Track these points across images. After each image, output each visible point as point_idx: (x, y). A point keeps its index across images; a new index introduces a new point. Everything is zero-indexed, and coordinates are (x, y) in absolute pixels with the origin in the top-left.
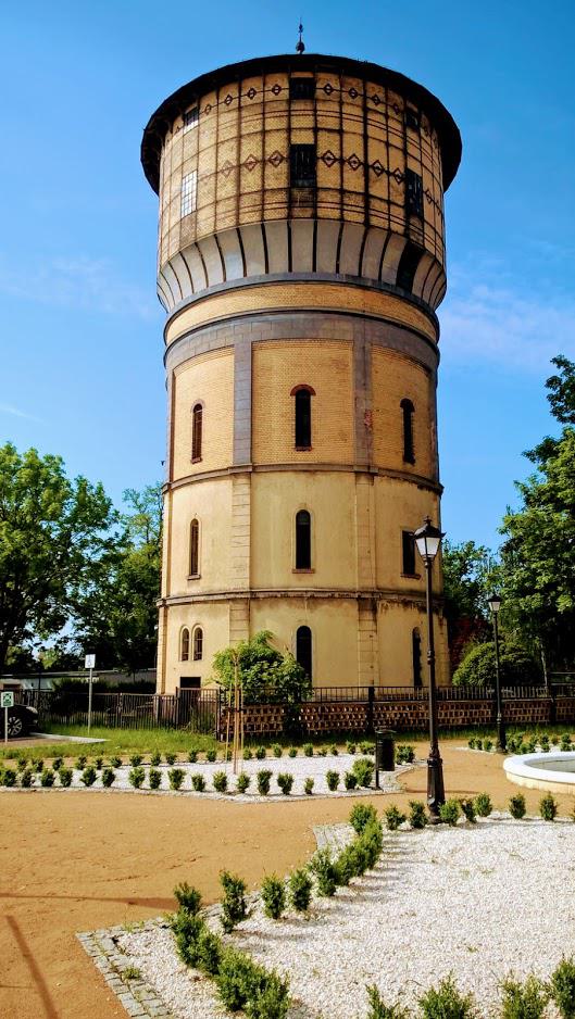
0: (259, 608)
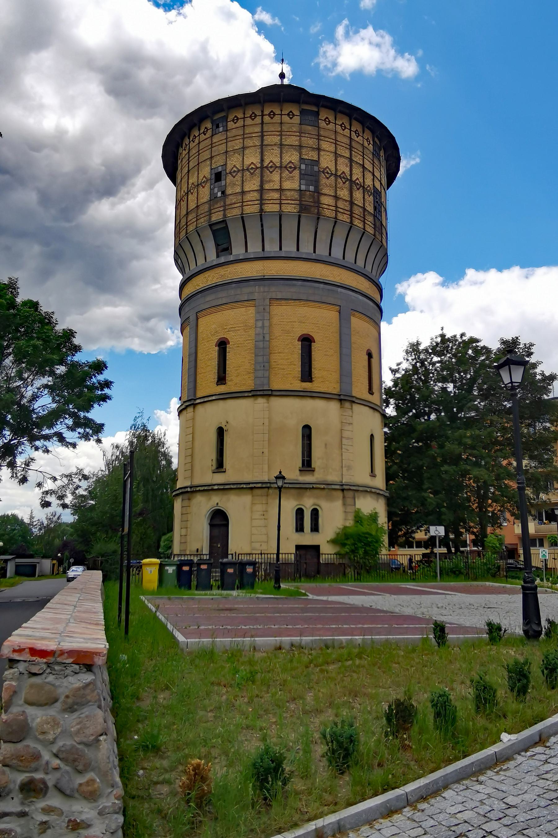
0: (358, 498)
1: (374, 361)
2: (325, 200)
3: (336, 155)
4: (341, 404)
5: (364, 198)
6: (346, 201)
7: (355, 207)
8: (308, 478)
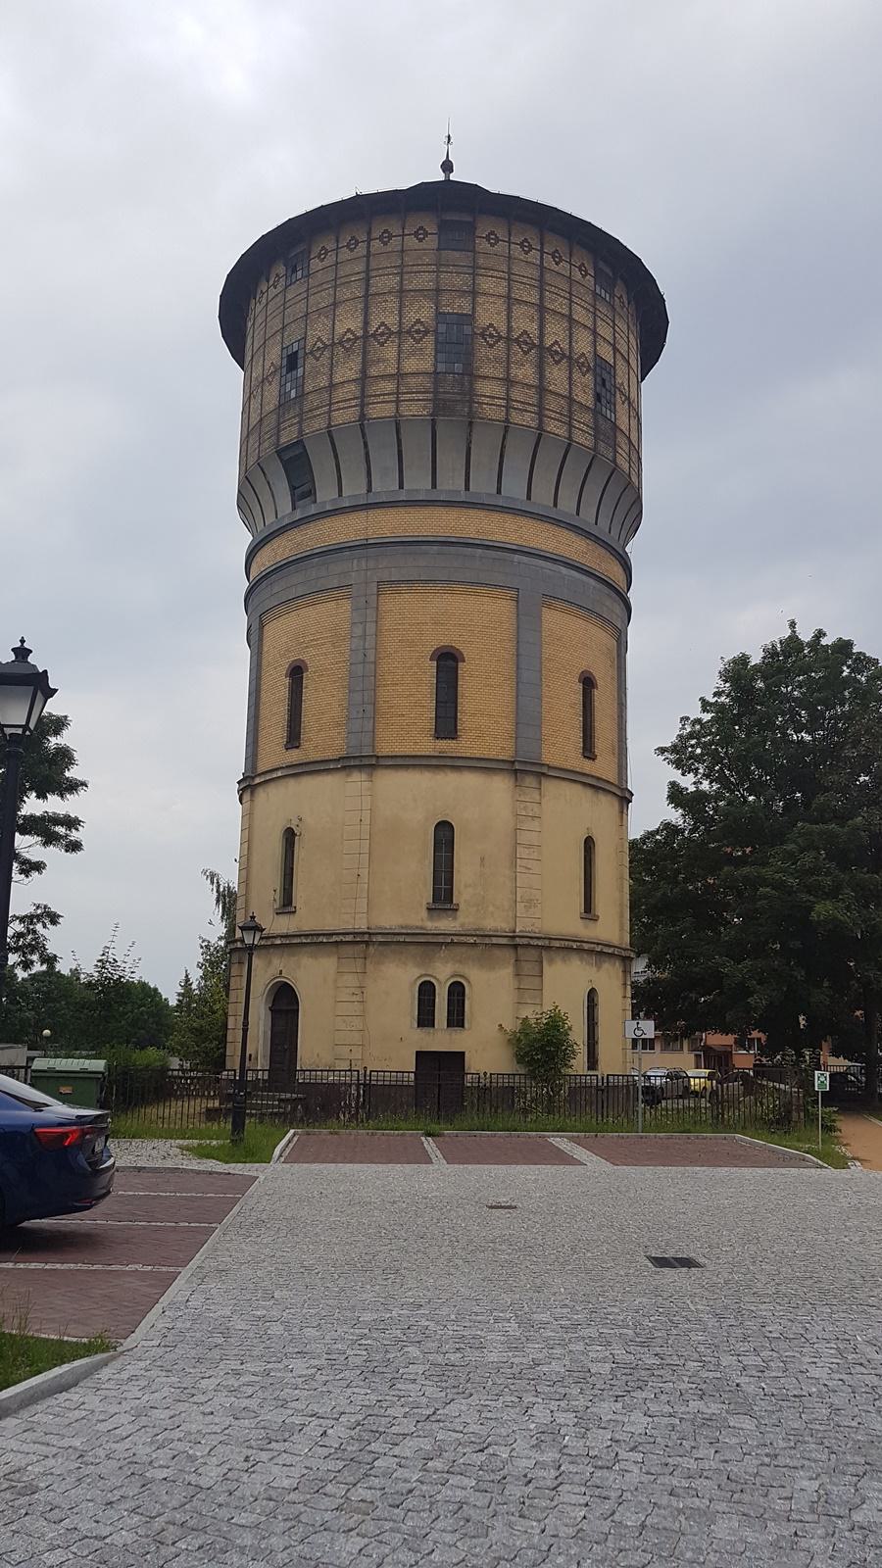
0: (551, 961)
1: (602, 697)
2: (485, 388)
3: (510, 300)
4: (516, 779)
5: (570, 378)
6: (529, 386)
7: (550, 397)
8: (445, 924)
